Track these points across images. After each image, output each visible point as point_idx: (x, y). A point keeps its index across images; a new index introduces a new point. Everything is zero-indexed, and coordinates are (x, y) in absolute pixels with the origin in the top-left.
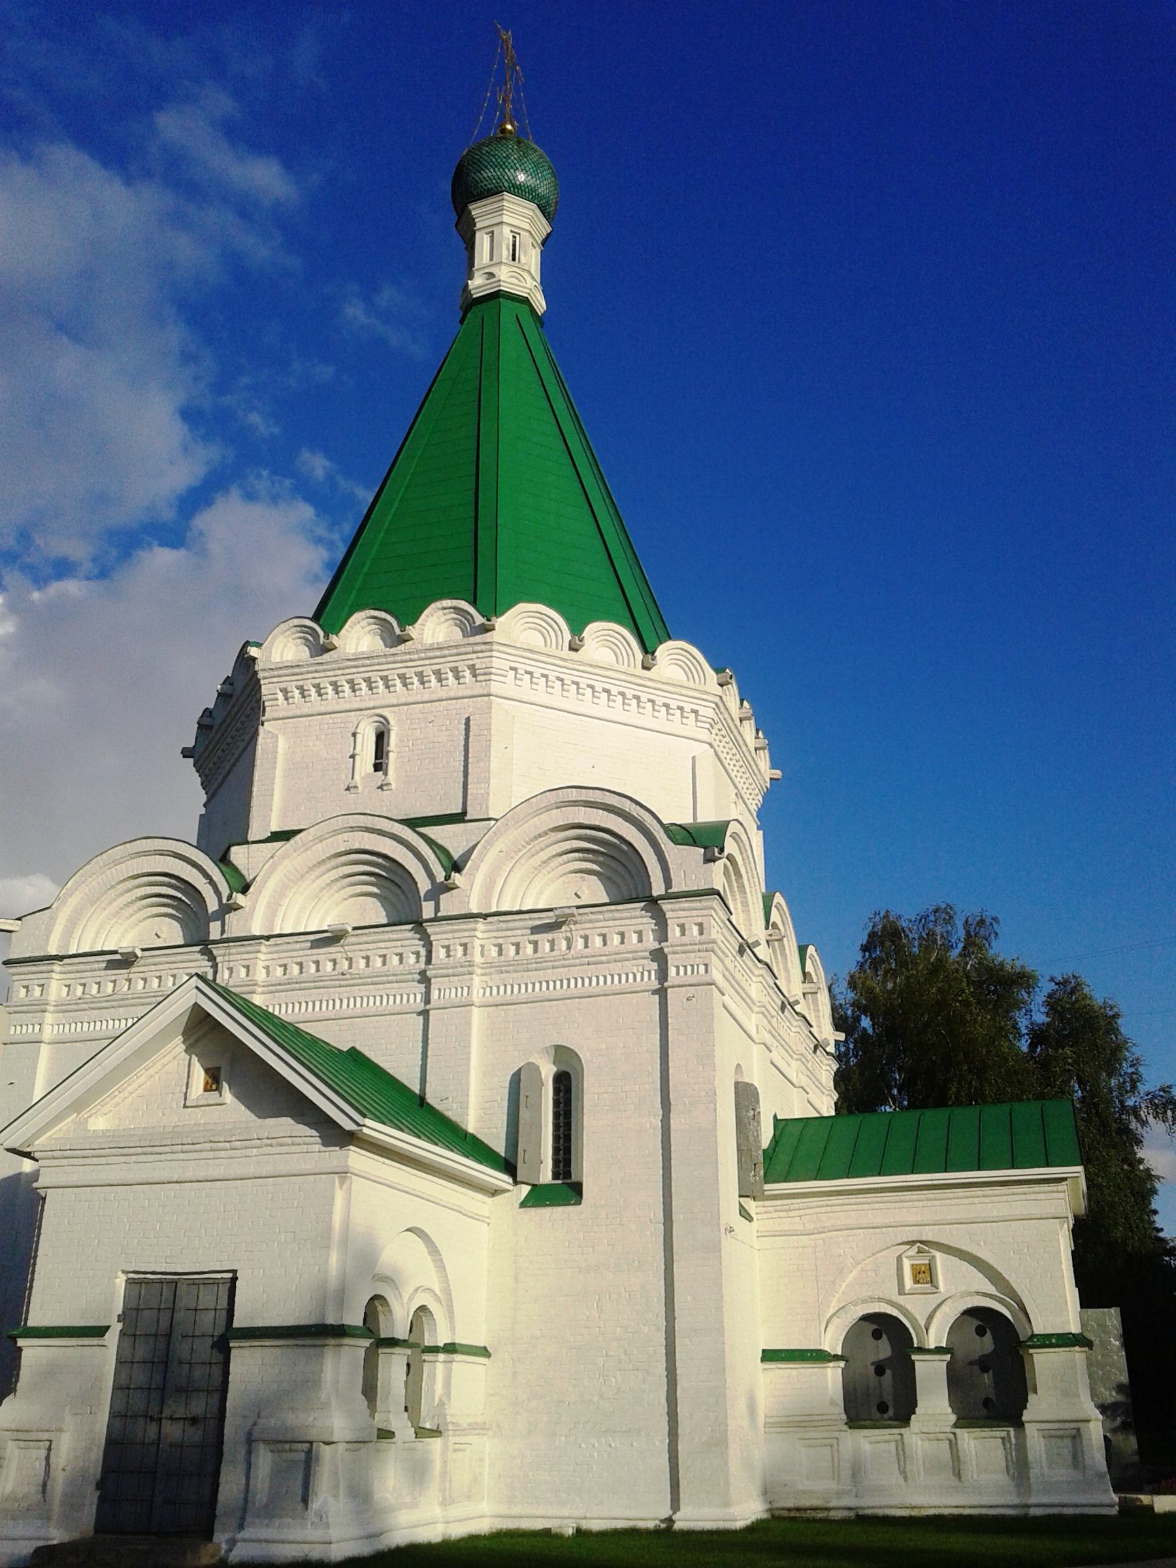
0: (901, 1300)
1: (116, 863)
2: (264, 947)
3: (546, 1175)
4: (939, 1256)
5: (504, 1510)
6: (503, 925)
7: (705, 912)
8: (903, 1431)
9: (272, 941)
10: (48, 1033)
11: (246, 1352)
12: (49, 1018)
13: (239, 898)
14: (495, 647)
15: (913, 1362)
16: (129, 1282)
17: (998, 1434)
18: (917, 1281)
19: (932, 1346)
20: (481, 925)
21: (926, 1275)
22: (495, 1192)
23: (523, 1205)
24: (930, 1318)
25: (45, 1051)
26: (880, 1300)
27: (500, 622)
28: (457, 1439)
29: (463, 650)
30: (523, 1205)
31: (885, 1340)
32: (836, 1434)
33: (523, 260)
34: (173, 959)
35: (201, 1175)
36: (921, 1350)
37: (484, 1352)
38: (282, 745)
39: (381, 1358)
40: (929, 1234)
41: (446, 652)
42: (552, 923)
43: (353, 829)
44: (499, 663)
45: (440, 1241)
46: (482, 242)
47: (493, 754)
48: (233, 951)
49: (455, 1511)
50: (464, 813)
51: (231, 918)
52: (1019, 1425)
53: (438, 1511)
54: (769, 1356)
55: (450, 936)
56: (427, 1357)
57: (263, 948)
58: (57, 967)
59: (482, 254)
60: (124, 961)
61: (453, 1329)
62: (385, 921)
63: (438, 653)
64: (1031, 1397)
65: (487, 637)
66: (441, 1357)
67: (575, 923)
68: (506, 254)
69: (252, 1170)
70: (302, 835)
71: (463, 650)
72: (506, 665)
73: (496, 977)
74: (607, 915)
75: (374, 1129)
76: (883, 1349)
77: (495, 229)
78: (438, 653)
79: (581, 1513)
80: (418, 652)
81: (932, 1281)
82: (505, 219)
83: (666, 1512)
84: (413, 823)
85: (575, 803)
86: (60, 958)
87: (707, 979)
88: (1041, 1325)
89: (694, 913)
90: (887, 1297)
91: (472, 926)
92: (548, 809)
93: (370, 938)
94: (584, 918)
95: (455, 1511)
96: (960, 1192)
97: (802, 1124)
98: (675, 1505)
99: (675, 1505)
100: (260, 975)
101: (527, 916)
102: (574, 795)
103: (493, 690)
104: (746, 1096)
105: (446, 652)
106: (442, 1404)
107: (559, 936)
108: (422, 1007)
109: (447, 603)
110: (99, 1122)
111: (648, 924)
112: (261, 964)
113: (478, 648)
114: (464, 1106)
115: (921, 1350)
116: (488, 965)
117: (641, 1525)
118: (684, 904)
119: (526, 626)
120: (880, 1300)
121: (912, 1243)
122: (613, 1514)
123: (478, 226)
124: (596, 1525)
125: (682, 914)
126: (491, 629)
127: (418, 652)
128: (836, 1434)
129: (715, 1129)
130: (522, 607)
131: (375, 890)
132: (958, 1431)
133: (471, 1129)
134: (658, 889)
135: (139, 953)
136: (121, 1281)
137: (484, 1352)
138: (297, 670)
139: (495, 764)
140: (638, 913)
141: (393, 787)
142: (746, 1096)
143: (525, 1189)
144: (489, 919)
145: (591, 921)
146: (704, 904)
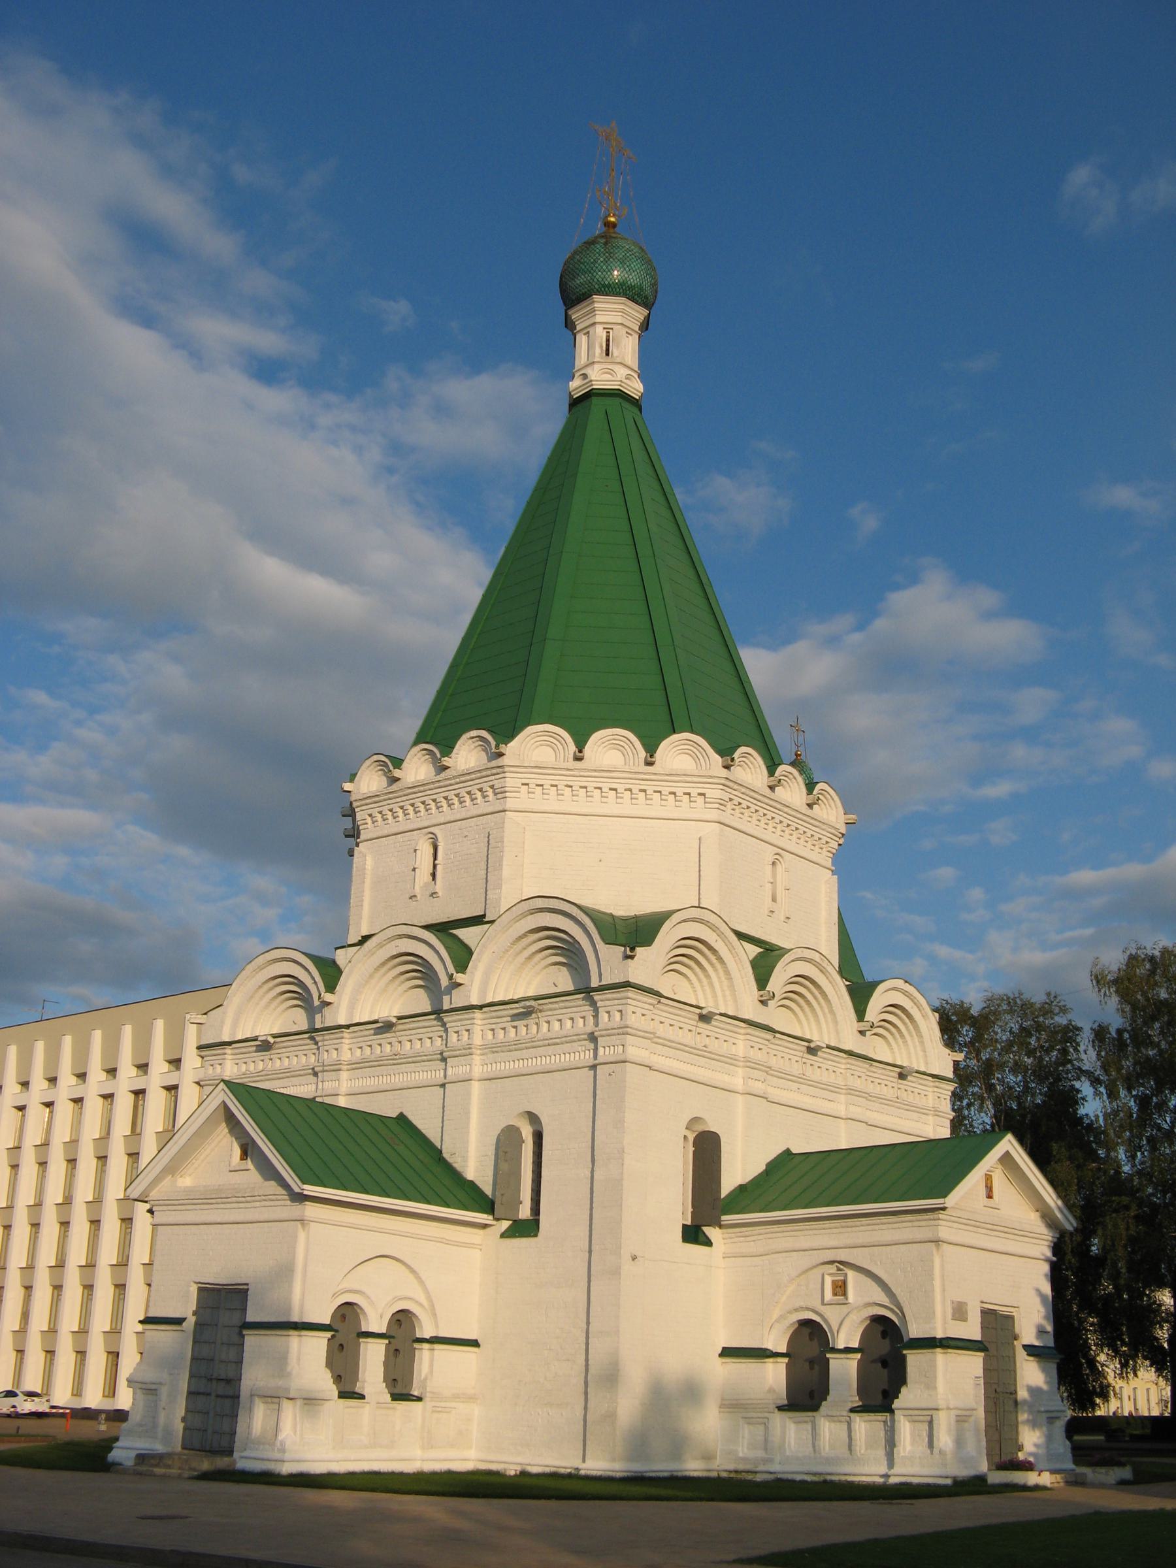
0: (822, 1309)
1: (261, 968)
2: (346, 1033)
3: (525, 1212)
4: (851, 1275)
5: (483, 1456)
6: (494, 1014)
7: (623, 1001)
8: (814, 1414)
9: (352, 1029)
10: (478, 1070)
11: (252, 1338)
12: (477, 1059)
13: (459, 978)
14: (507, 769)
15: (904, 1357)
16: (200, 1289)
17: (880, 1418)
18: (835, 1294)
19: (841, 1346)
20: (478, 1014)
21: (840, 1288)
22: (485, 1226)
23: (503, 1236)
24: (841, 1324)
25: (476, 1087)
26: (808, 1309)
27: (513, 748)
28: (434, 1404)
29: (484, 773)
30: (503, 1236)
31: (810, 1339)
32: (766, 1415)
33: (615, 354)
34: (244, 1050)
35: (232, 1219)
36: (834, 1350)
37: (475, 1343)
38: (370, 863)
39: (362, 1346)
40: (842, 1255)
41: (473, 776)
42: (525, 1010)
43: (400, 936)
44: (511, 781)
45: (429, 1265)
46: (582, 340)
47: (505, 863)
48: (327, 1037)
49: (433, 1454)
50: (484, 916)
51: (326, 1010)
52: (892, 1411)
53: (418, 1453)
54: (727, 1352)
55: (459, 1024)
56: (416, 1345)
57: (345, 1035)
58: (228, 1050)
59: (581, 358)
60: (386, 1027)
61: (437, 1326)
62: (571, 987)
63: (468, 777)
64: (904, 1390)
65: (499, 762)
66: (426, 1346)
67: (541, 1011)
68: (598, 351)
69: (256, 1217)
70: (374, 938)
71: (484, 773)
72: (518, 783)
73: (491, 1056)
74: (562, 1005)
75: (310, 1190)
76: (884, 1347)
77: (591, 330)
78: (468, 777)
79: (527, 1462)
80: (455, 777)
81: (845, 1294)
82: (598, 319)
83: (883, 1469)
84: (442, 929)
85: (541, 910)
86: (230, 1043)
87: (622, 1058)
88: (915, 1330)
89: (616, 1002)
90: (810, 1305)
91: (471, 1015)
92: (524, 915)
93: (411, 1026)
94: (545, 1007)
95: (433, 1454)
96: (864, 1221)
97: (845, 1153)
98: (891, 1464)
99: (891, 1464)
100: (477, 1040)
101: (508, 1006)
102: (540, 903)
103: (508, 807)
104: (706, 1150)
105: (473, 776)
106: (426, 1379)
107: (531, 1021)
108: (592, 1062)
109: (474, 733)
110: (186, 1181)
111: (588, 1011)
112: (346, 1047)
113: (494, 771)
114: (465, 1159)
115: (834, 1350)
116: (484, 1047)
117: (562, 1471)
118: (608, 995)
119: (538, 745)
120: (808, 1309)
121: (832, 1262)
122: (547, 1463)
123: (578, 328)
124: (534, 1470)
125: (608, 1003)
126: (501, 755)
127: (455, 777)
128: (766, 1415)
129: (622, 1179)
130: (530, 729)
131: (420, 982)
132: (852, 1415)
133: (470, 1175)
134: (594, 983)
135: (272, 1040)
136: (194, 1289)
137: (475, 1343)
138: (377, 799)
139: (506, 872)
140: (581, 1002)
141: (440, 894)
142: (706, 1150)
143: (505, 1224)
144: (485, 1009)
145: (551, 1010)
146: (622, 995)
